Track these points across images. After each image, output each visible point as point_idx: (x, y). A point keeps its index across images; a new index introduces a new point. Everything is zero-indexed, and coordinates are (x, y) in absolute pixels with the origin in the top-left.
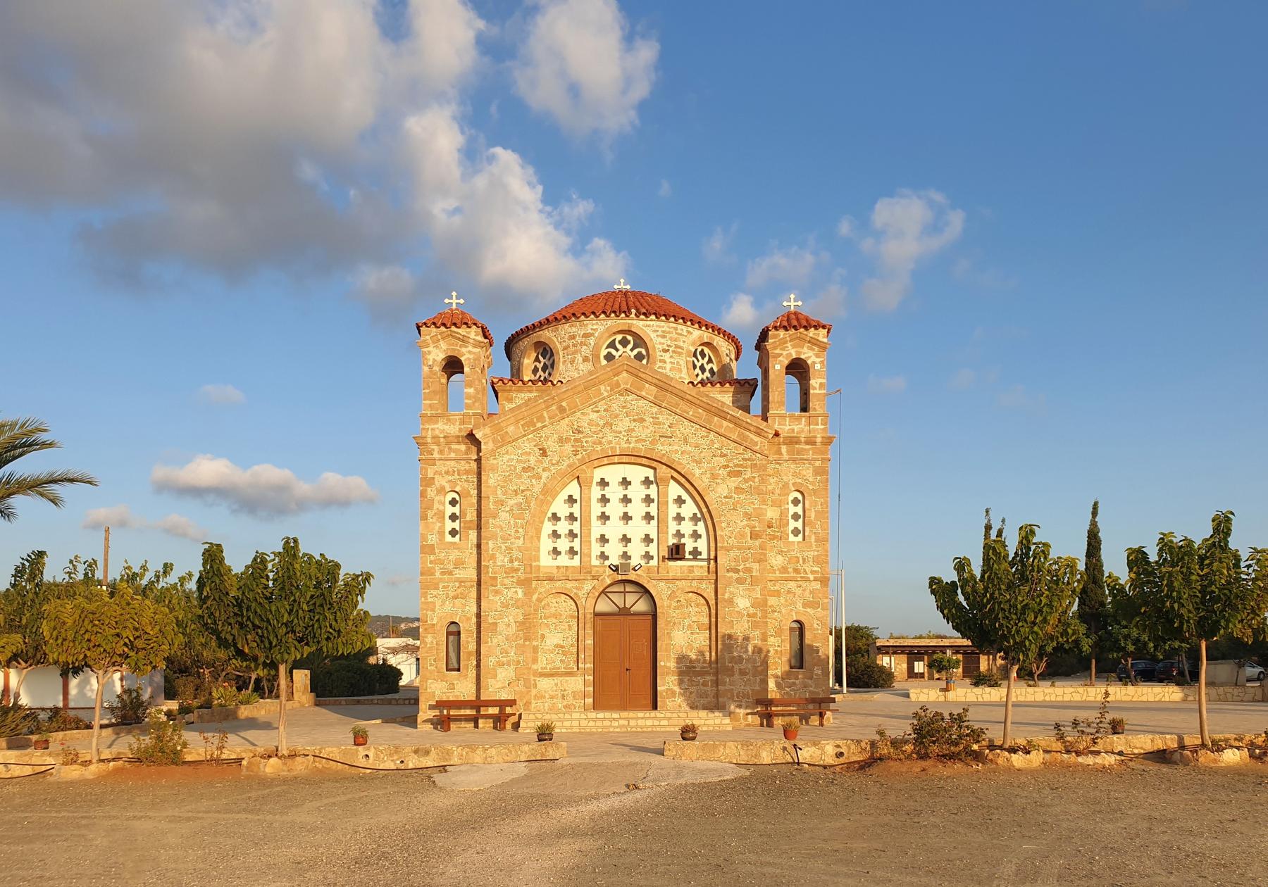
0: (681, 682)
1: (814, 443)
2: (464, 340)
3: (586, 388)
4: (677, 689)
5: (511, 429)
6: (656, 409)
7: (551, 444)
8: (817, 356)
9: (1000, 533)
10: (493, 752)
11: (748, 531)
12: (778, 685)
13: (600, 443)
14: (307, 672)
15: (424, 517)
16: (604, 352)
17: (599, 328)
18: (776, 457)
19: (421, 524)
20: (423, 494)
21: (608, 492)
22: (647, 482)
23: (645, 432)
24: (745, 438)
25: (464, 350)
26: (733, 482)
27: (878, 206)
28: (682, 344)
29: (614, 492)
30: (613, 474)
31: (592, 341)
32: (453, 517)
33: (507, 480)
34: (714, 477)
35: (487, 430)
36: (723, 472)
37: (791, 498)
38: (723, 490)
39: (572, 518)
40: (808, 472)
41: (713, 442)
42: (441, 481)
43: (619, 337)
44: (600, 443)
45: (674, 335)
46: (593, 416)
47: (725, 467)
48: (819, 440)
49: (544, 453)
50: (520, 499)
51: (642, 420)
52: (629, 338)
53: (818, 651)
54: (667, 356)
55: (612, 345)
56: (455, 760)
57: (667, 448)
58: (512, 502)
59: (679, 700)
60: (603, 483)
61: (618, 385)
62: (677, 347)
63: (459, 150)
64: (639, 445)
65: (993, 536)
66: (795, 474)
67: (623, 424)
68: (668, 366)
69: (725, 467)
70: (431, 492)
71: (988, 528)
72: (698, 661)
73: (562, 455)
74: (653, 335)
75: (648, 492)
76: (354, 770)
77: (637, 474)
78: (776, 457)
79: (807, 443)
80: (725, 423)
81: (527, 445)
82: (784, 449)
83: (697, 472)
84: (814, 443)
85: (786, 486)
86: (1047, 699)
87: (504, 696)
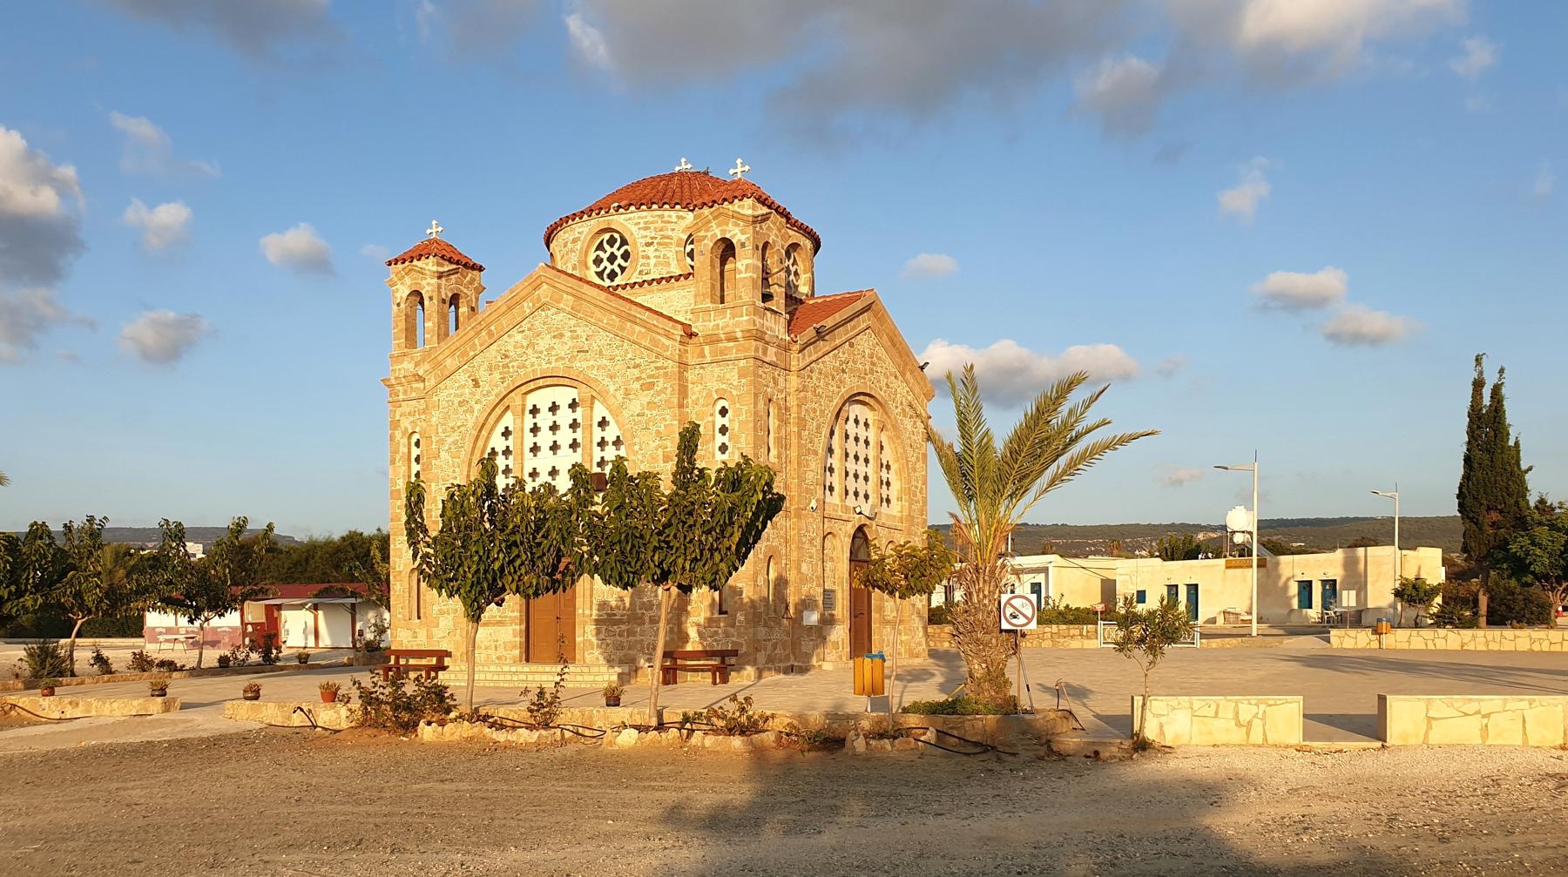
0: (598, 632)
1: (735, 339)
2: (422, 272)
3: (510, 308)
4: (594, 639)
5: (449, 361)
6: (573, 322)
7: (482, 374)
8: (743, 233)
9: (1496, 390)
10: (115, 705)
11: (660, 451)
12: (700, 634)
13: (524, 366)
14: (1439, 551)
15: (393, 462)
16: (592, 256)
17: (583, 230)
18: (699, 360)
19: (391, 468)
20: (392, 438)
21: (539, 419)
22: (573, 405)
23: (562, 349)
24: (655, 342)
25: (424, 283)
26: (645, 397)
27: (24, 142)
28: (670, 233)
29: (545, 419)
30: (542, 398)
31: (579, 245)
32: (723, 430)
33: (446, 417)
34: (627, 394)
35: (427, 366)
36: (637, 386)
37: (718, 408)
38: (635, 406)
39: (507, 452)
40: (733, 376)
41: (627, 352)
42: (406, 423)
43: (607, 236)
44: (524, 366)
45: (660, 225)
46: (518, 337)
47: (638, 379)
48: (739, 335)
49: (476, 383)
50: (456, 436)
51: (562, 335)
52: (616, 236)
53: (741, 593)
54: (650, 251)
55: (600, 247)
56: (93, 713)
57: (585, 365)
58: (450, 440)
59: (597, 652)
60: (535, 411)
61: (539, 299)
62: (664, 237)
63: (8, 129)
64: (560, 364)
65: (1487, 393)
66: (720, 379)
67: (544, 342)
68: (652, 261)
69: (638, 379)
70: (398, 434)
71: (1478, 385)
72: (618, 607)
73: (494, 385)
74: (634, 229)
75: (574, 416)
76: (63, 727)
77: (564, 396)
78: (699, 360)
79: (729, 340)
80: (637, 328)
81: (462, 377)
82: (707, 349)
83: (612, 388)
84: (735, 339)
85: (709, 395)
86: (1536, 647)
87: (444, 646)
